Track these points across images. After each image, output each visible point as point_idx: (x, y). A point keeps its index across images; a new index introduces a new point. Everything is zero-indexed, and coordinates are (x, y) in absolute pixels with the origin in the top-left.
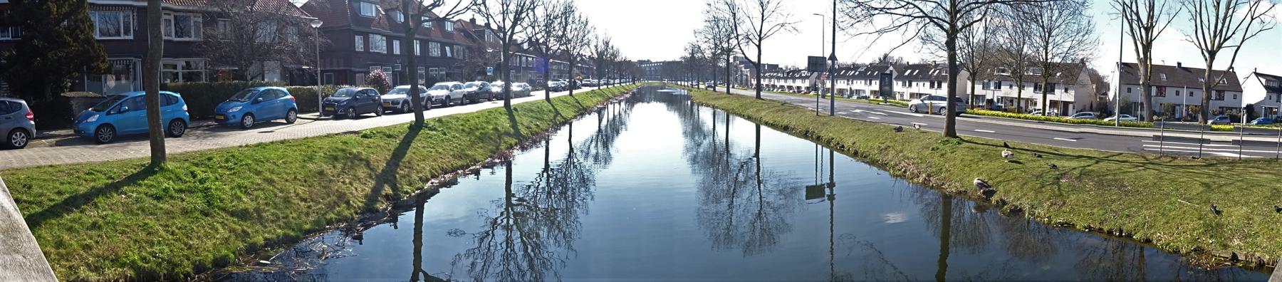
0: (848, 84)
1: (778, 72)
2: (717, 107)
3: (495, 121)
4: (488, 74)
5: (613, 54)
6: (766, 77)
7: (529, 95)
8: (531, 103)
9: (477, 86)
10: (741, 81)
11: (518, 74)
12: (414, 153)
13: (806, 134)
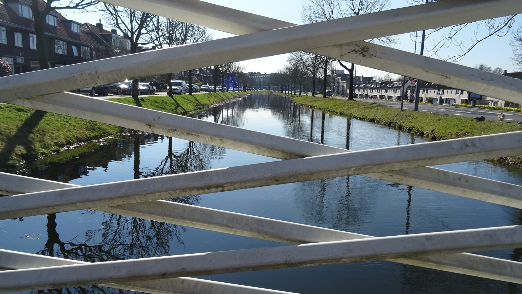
0: (438, 93)
1: (371, 83)
6: (361, 88)
10: (338, 91)
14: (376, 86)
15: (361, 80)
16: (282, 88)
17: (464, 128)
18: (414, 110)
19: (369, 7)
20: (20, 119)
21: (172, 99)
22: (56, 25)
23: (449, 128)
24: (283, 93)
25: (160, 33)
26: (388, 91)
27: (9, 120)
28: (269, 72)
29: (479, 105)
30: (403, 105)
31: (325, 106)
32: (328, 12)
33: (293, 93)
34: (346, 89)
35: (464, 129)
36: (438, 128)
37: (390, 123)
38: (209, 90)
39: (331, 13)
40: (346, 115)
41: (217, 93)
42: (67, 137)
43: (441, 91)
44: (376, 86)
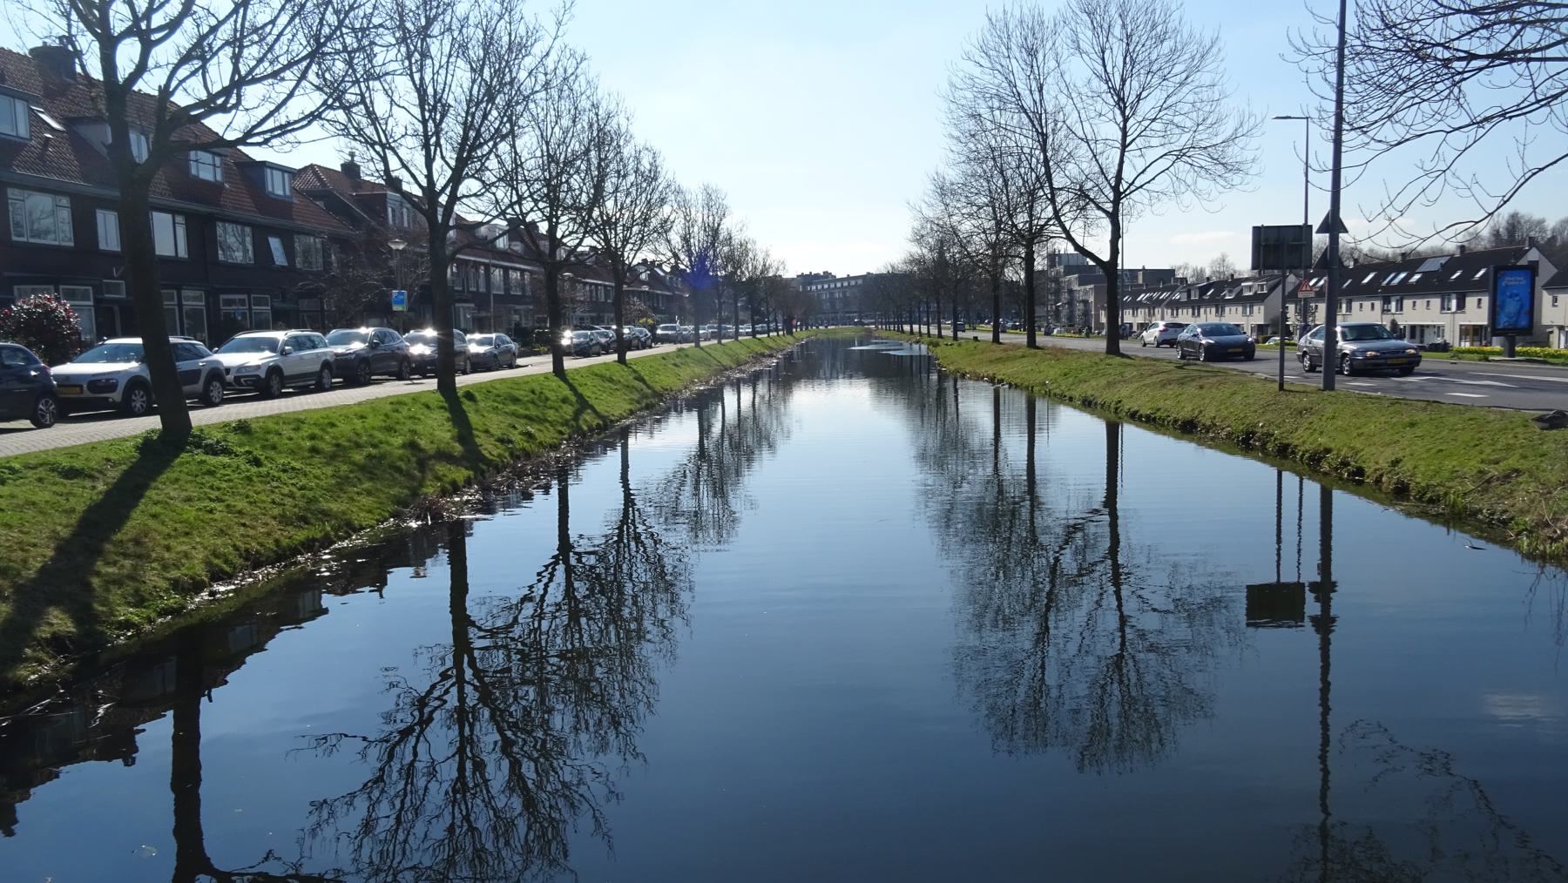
0: (1385, 311)
1: (1173, 289)
2: (1000, 381)
3: (410, 425)
4: (395, 308)
5: (730, 258)
6: (1141, 305)
7: (511, 366)
8: (515, 382)
9: (363, 339)
10: (1071, 317)
11: (483, 314)
12: (154, 516)
13: (1246, 441)
14: (1189, 296)
15: (1140, 282)
16: (900, 316)
17: (1503, 454)
18: (1321, 386)
19: (1155, 68)
20: (68, 506)
21: (562, 383)
22: (219, 178)
23: (1450, 456)
24: (903, 332)
25: (523, 188)
26: (1227, 309)
27: (30, 513)
28: (859, 270)
29: (1525, 349)
30: (1286, 364)
31: (1034, 379)
32: (1028, 92)
33: (934, 331)
34: (1097, 310)
35: (1505, 459)
36: (1412, 455)
37: (1248, 434)
38: (679, 338)
39: (1037, 96)
40: (1103, 406)
41: (702, 349)
42: (216, 555)
43: (1393, 304)
44: (1189, 296)
